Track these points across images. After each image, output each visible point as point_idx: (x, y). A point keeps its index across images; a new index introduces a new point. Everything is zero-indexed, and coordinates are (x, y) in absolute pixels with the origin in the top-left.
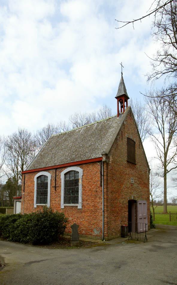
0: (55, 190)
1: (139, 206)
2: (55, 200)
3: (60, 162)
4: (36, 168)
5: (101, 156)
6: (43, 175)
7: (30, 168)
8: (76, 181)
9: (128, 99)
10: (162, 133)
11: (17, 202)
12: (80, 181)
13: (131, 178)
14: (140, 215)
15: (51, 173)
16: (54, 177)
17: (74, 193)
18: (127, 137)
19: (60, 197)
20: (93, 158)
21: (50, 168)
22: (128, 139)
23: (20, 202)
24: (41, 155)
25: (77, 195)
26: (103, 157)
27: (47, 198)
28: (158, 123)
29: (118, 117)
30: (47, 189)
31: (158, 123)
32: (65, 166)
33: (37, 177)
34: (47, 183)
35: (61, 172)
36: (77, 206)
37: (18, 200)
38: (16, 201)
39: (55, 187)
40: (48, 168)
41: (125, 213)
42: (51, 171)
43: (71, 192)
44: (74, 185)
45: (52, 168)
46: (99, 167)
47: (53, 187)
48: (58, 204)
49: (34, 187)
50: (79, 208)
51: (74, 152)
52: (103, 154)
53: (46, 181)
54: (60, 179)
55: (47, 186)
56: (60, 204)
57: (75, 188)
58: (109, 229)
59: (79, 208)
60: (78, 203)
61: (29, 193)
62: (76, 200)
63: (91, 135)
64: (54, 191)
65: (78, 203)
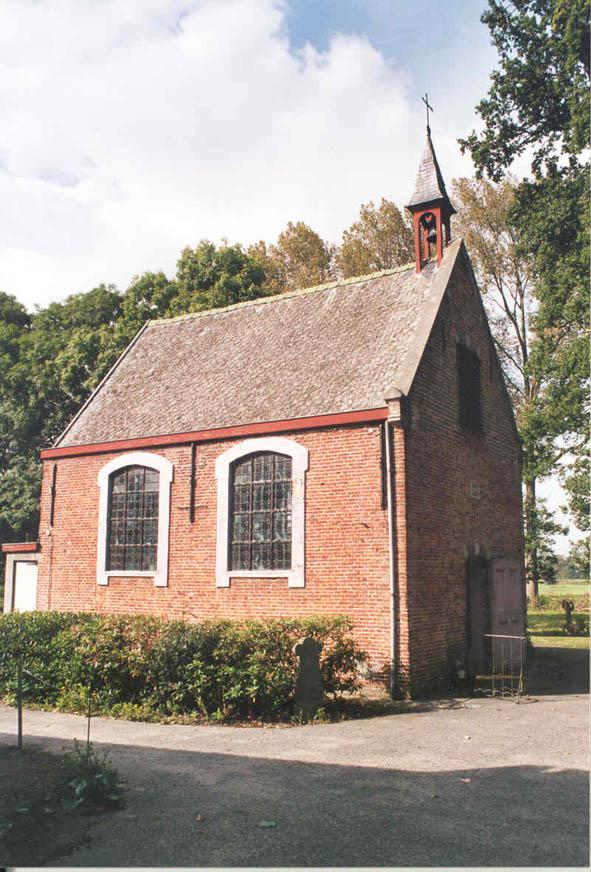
0: (192, 520)
1: (496, 576)
2: (191, 558)
3: (205, 421)
4: (100, 440)
5: (385, 405)
6: (136, 467)
7: (76, 438)
8: (279, 487)
9: (450, 215)
10: (516, 325)
11: (18, 564)
12: (298, 490)
13: (471, 484)
14: (501, 610)
15: (171, 460)
16: (188, 472)
17: (273, 532)
18: (458, 341)
19: (212, 545)
20: (344, 408)
21: (168, 440)
22: (461, 347)
23: (35, 562)
24: (115, 391)
25: (281, 536)
26: (391, 408)
27: (155, 549)
28: (501, 290)
29: (417, 272)
30: (157, 515)
31: (501, 290)
32: (234, 433)
33: (112, 471)
34: (155, 496)
35: (214, 456)
36: (286, 578)
37: (23, 557)
38: (15, 562)
39: (193, 510)
40: (160, 442)
41: (458, 604)
42: (173, 451)
43: (257, 526)
44: (269, 501)
45: (177, 440)
46: (377, 441)
47: (181, 509)
48: (205, 570)
49: (96, 507)
50: (291, 583)
51: (259, 387)
52: (392, 397)
53: (149, 488)
54: (214, 481)
55: (156, 505)
56: (211, 573)
57: (278, 515)
58: (75, 710)
59: (291, 583)
60: (288, 566)
61: (74, 531)
62: (279, 556)
63: (321, 327)
64: (187, 521)
65: (288, 566)
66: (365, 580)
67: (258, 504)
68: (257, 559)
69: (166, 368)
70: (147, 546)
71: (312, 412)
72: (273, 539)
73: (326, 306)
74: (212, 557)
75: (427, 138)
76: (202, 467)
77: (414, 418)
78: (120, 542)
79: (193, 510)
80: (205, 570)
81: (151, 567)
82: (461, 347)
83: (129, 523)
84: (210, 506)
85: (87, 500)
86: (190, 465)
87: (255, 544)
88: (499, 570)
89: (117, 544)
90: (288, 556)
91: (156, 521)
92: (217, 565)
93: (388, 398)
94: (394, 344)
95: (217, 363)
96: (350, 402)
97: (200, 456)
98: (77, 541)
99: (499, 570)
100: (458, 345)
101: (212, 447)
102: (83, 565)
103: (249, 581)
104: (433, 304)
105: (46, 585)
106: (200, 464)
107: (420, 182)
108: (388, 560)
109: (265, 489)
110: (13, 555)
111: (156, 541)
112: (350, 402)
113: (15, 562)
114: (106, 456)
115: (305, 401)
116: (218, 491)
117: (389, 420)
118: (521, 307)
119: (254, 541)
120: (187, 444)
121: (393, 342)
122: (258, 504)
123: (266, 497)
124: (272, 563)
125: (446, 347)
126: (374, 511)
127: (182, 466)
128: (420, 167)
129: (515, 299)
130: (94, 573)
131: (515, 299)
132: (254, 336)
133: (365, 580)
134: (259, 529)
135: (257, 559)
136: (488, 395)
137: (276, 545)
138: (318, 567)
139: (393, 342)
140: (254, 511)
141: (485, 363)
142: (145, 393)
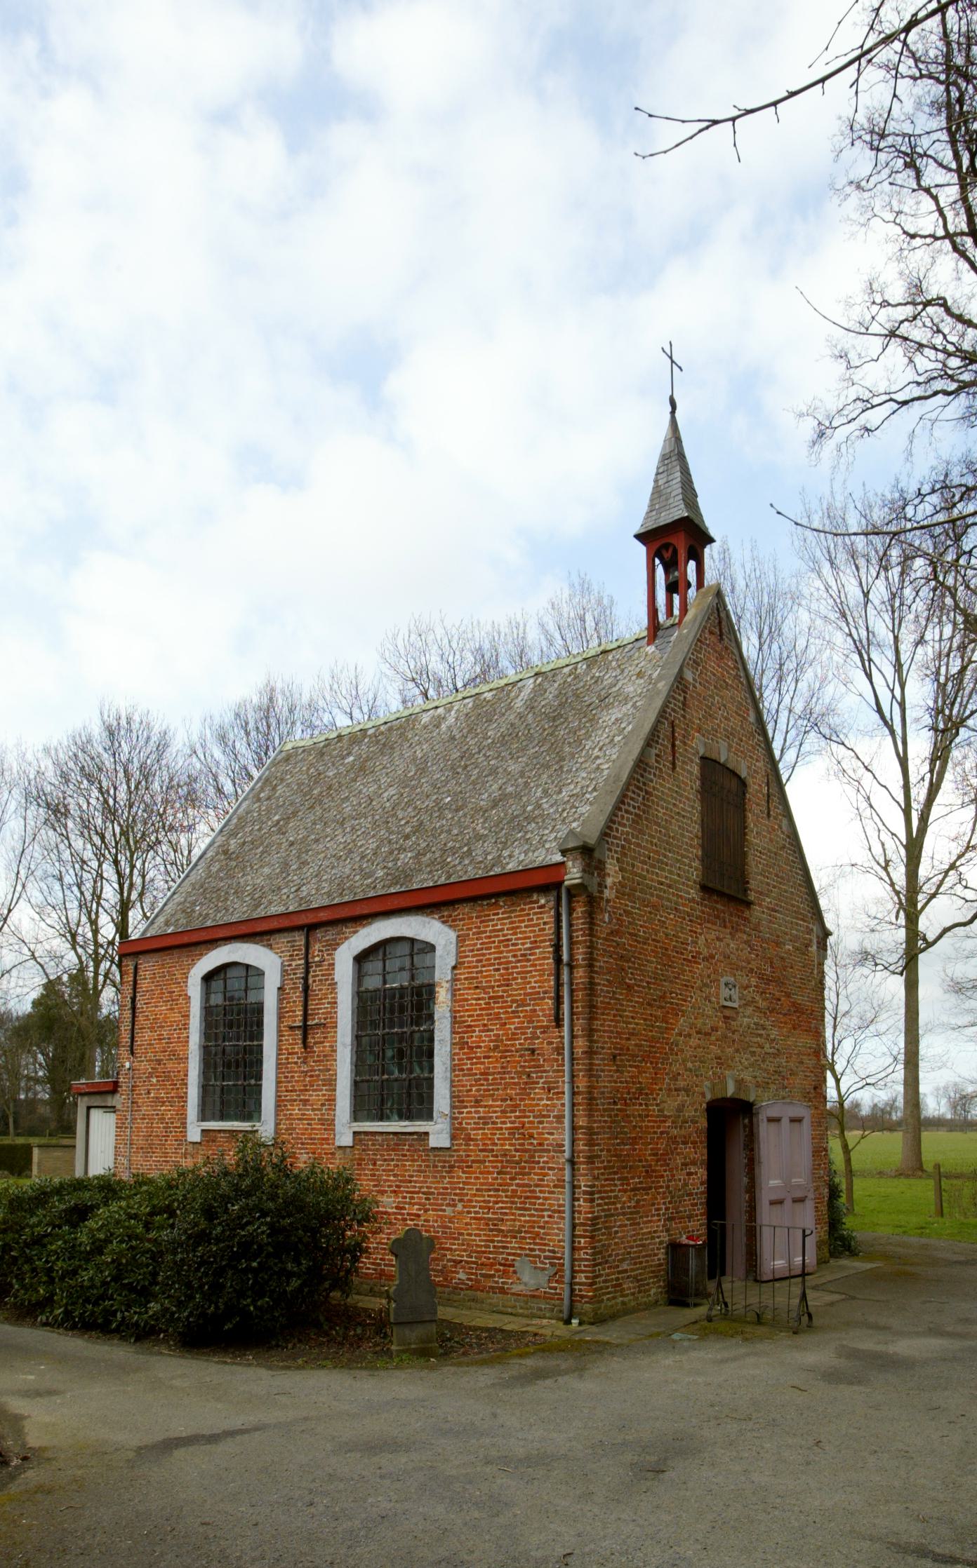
2: (305, 1102)
3: (329, 894)
4: (196, 924)
7: (167, 923)
8: (419, 994)
12: (443, 996)
14: (774, 1182)
19: (331, 1083)
21: (275, 924)
22: (709, 763)
24: (225, 852)
25: (422, 1069)
26: (570, 864)
29: (649, 644)
31: (869, 676)
32: (359, 911)
34: (259, 1009)
35: (334, 946)
37: (97, 1101)
38: (89, 1108)
42: (282, 940)
43: (389, 1053)
45: (286, 923)
46: (549, 917)
47: (292, 1028)
49: (186, 1027)
50: (433, 1142)
51: (407, 837)
53: (252, 998)
54: (333, 985)
55: (260, 1024)
56: (329, 1124)
57: (417, 1036)
59: (433, 1142)
61: (159, 1062)
64: (298, 1048)
66: (531, 1136)
67: (391, 1020)
68: (389, 1104)
69: (295, 814)
70: (249, 1085)
71: (472, 873)
72: (411, 1072)
73: (519, 704)
74: (332, 1100)
75: (668, 416)
76: (320, 964)
77: (609, 881)
78: (400, 1072)
79: (305, 1029)
80: (322, 1121)
81: (255, 1115)
82: (709, 763)
83: (228, 1049)
84: (329, 1025)
85: (176, 1016)
86: (302, 962)
87: (387, 1080)
88: (770, 1120)
89: (396, 1074)
90: (429, 1099)
91: (261, 1046)
92: (337, 1112)
93: (563, 848)
94: (598, 762)
95: (360, 804)
96: (522, 856)
97: (316, 947)
98: (166, 1077)
99: (770, 1120)
100: (703, 758)
101: (330, 934)
102: (168, 1112)
103: (379, 1138)
104: (659, 692)
105: (123, 1143)
106: (317, 959)
107: (657, 493)
108: (563, 1105)
109: (402, 997)
110: (86, 1099)
111: (261, 1079)
112: (522, 856)
113: (89, 1108)
114: (203, 947)
115: (462, 858)
116: (339, 1001)
117: (566, 883)
118: (902, 705)
119: (386, 1077)
120: (298, 928)
121: (598, 757)
122: (391, 1020)
123: (402, 1009)
124: (409, 1110)
125: (678, 764)
126: (545, 1030)
127: (294, 963)
128: (658, 468)
129: (892, 691)
130: (184, 1125)
131: (892, 691)
132: (415, 759)
133: (531, 1136)
134: (393, 1057)
135: (389, 1104)
136: (758, 835)
137: (414, 1082)
138: (470, 1115)
139: (598, 757)
140: (387, 1030)
141: (756, 787)
142: (263, 853)
